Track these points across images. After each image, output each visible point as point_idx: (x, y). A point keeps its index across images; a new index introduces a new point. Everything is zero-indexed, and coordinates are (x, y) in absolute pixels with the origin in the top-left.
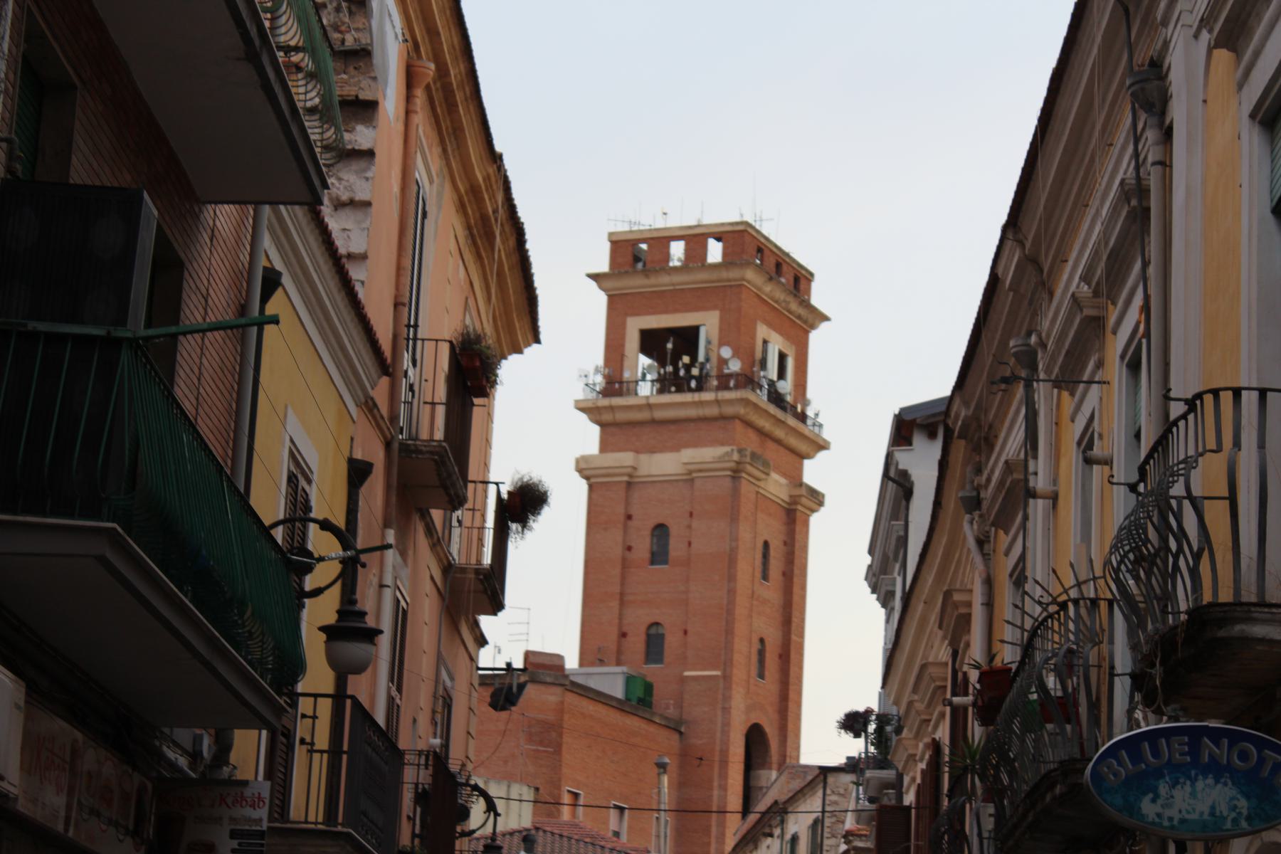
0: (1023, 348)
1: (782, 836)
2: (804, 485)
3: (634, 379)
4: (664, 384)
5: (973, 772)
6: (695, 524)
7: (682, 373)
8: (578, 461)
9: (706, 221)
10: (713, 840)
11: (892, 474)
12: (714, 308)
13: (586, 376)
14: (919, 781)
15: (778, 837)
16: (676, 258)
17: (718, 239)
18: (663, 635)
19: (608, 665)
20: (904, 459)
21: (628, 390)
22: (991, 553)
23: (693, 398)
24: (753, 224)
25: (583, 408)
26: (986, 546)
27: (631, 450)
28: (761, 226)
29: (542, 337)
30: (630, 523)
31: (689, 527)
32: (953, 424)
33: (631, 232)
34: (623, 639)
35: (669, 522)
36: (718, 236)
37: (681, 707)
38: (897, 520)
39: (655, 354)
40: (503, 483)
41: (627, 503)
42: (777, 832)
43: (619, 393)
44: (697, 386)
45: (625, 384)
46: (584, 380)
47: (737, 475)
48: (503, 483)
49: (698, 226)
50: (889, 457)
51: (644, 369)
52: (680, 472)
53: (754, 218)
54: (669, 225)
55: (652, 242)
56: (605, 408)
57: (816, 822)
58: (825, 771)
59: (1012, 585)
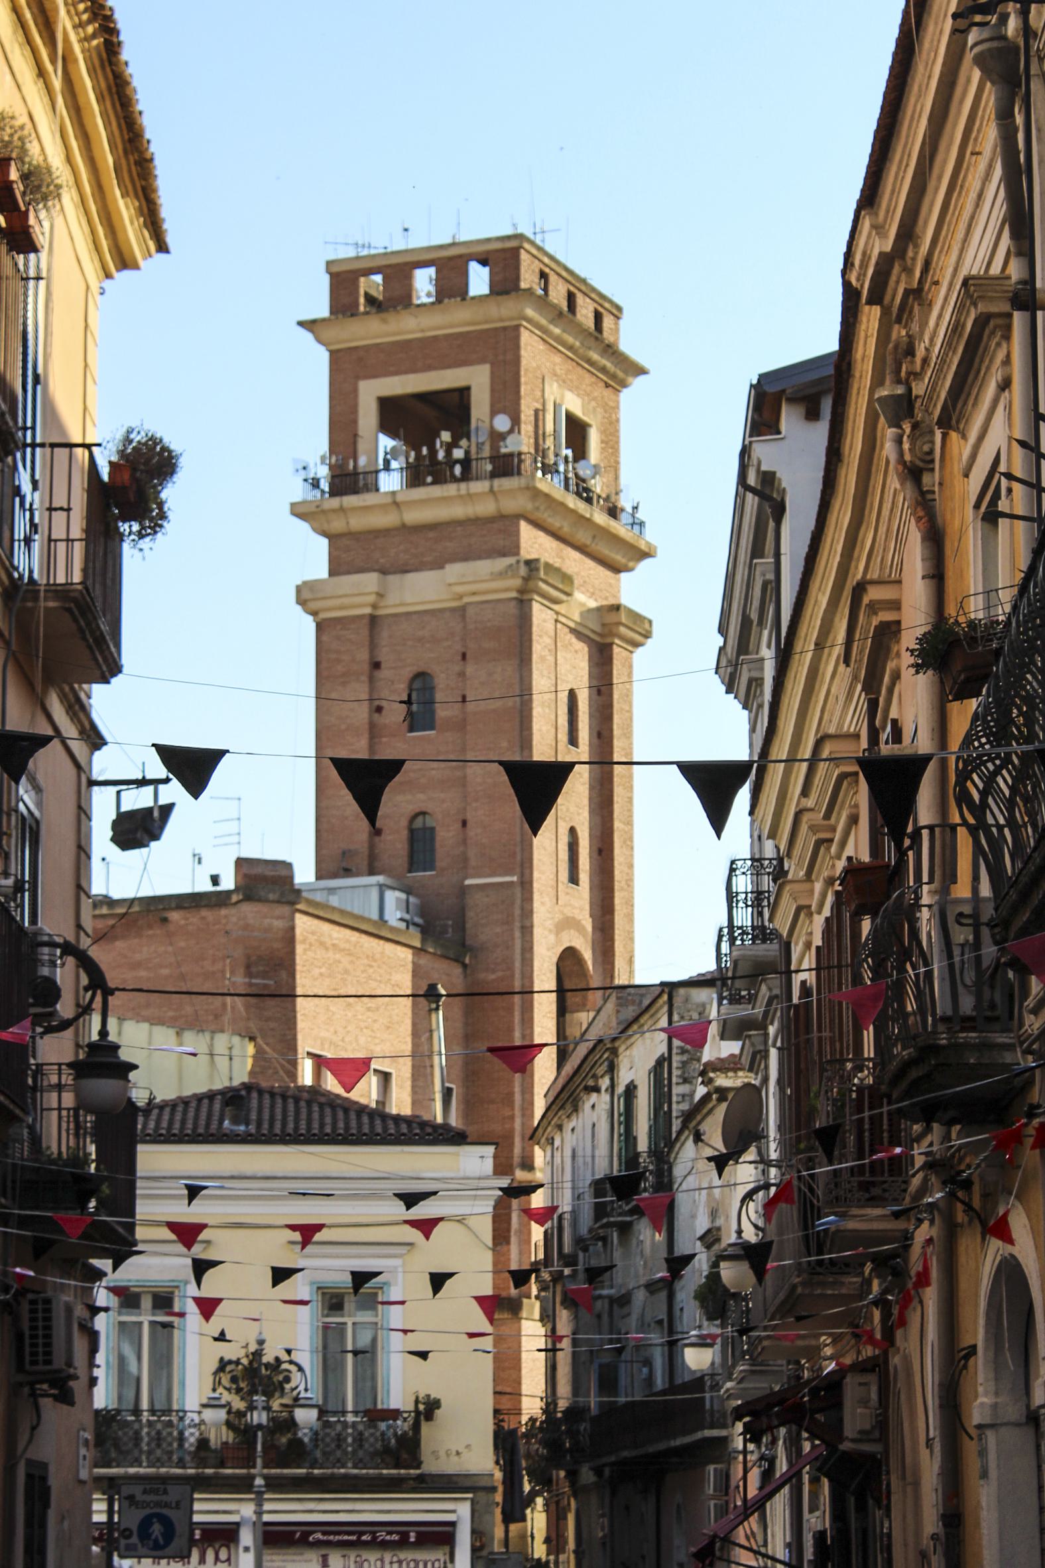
0: (995, 44)
1: (612, 1088)
2: (622, 609)
3: (372, 469)
4: (415, 477)
5: (909, 887)
6: (470, 669)
7: (441, 455)
8: (299, 589)
9: (463, 237)
10: (517, 1112)
11: (752, 480)
12: (482, 361)
13: (304, 468)
14: (818, 941)
15: (606, 1090)
16: (423, 294)
17: (484, 262)
18: (432, 829)
19: (358, 875)
20: (767, 454)
21: (366, 485)
22: (936, 489)
23: (459, 490)
24: (531, 237)
25: (299, 511)
26: (926, 479)
27: (374, 571)
28: (543, 241)
29: (170, 240)
30: (377, 674)
31: (462, 674)
32: (858, 280)
33: (358, 258)
34: (377, 839)
35: (435, 669)
36: (484, 257)
37: (464, 929)
38: (762, 557)
39: (402, 432)
40: (99, 445)
41: (373, 646)
42: (605, 1083)
43: (355, 491)
44: (462, 473)
45: (361, 476)
46: (303, 474)
47: (526, 597)
48: (99, 445)
49: (453, 244)
50: (745, 452)
51: (386, 453)
52: (444, 597)
53: (532, 230)
54: (411, 246)
55: (389, 271)
56: (334, 511)
57: (660, 1062)
58: (670, 988)
59: (979, 523)
